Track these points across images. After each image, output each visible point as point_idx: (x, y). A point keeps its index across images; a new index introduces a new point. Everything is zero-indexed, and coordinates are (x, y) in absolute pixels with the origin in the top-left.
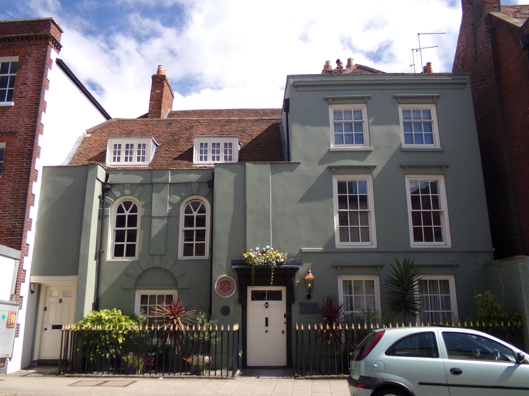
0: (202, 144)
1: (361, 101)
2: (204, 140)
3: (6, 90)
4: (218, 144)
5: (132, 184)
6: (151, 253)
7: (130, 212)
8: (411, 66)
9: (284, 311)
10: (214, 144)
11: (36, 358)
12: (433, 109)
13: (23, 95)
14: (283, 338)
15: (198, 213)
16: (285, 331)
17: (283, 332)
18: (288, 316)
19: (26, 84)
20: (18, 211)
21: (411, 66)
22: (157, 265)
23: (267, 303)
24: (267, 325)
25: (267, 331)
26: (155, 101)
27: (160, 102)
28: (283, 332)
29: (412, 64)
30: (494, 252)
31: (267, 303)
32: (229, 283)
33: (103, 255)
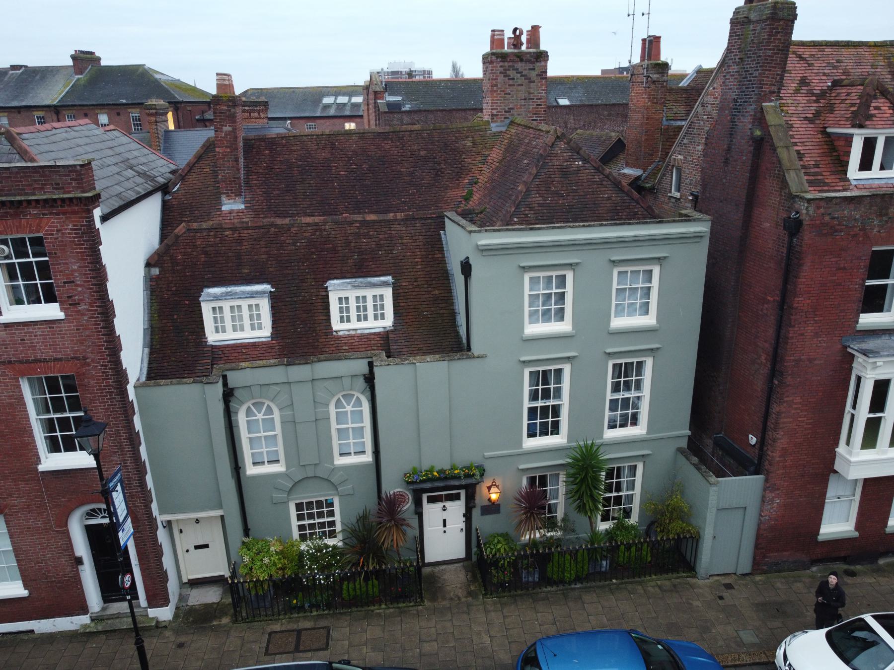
0: (340, 299)
1: (570, 267)
2: (343, 295)
3: (36, 280)
4: (364, 298)
5: (261, 385)
6: (301, 464)
7: (263, 415)
8: (643, 14)
9: (463, 511)
10: (357, 298)
11: (185, 580)
12: (656, 271)
13: (75, 300)
14: (462, 537)
15: (353, 407)
16: (464, 530)
17: (462, 529)
18: (468, 516)
19: (73, 282)
20: (128, 460)
21: (643, 14)
22: (310, 474)
23: (444, 506)
24: (445, 526)
25: (445, 532)
26: (226, 147)
27: (234, 149)
28: (462, 529)
29: (646, 12)
30: (689, 436)
31: (444, 506)
32: (404, 496)
33: (241, 471)
